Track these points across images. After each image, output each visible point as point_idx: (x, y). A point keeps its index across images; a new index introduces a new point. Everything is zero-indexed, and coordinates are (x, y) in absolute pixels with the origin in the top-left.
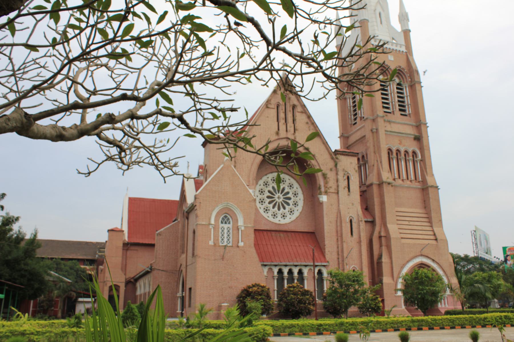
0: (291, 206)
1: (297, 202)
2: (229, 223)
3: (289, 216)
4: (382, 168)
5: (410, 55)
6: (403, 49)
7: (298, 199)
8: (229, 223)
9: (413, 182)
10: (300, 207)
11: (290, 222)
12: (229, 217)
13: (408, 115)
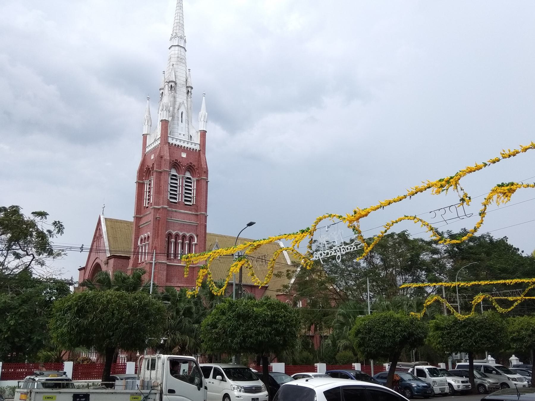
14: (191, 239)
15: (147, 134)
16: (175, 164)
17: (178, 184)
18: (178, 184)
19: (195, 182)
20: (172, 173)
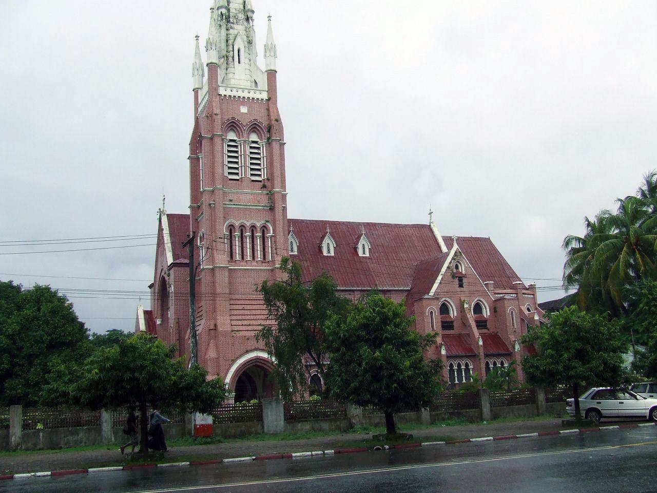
14: (244, 230)
15: (198, 88)
16: (254, 126)
17: (262, 153)
18: (262, 153)
19: (265, 147)
20: (251, 139)
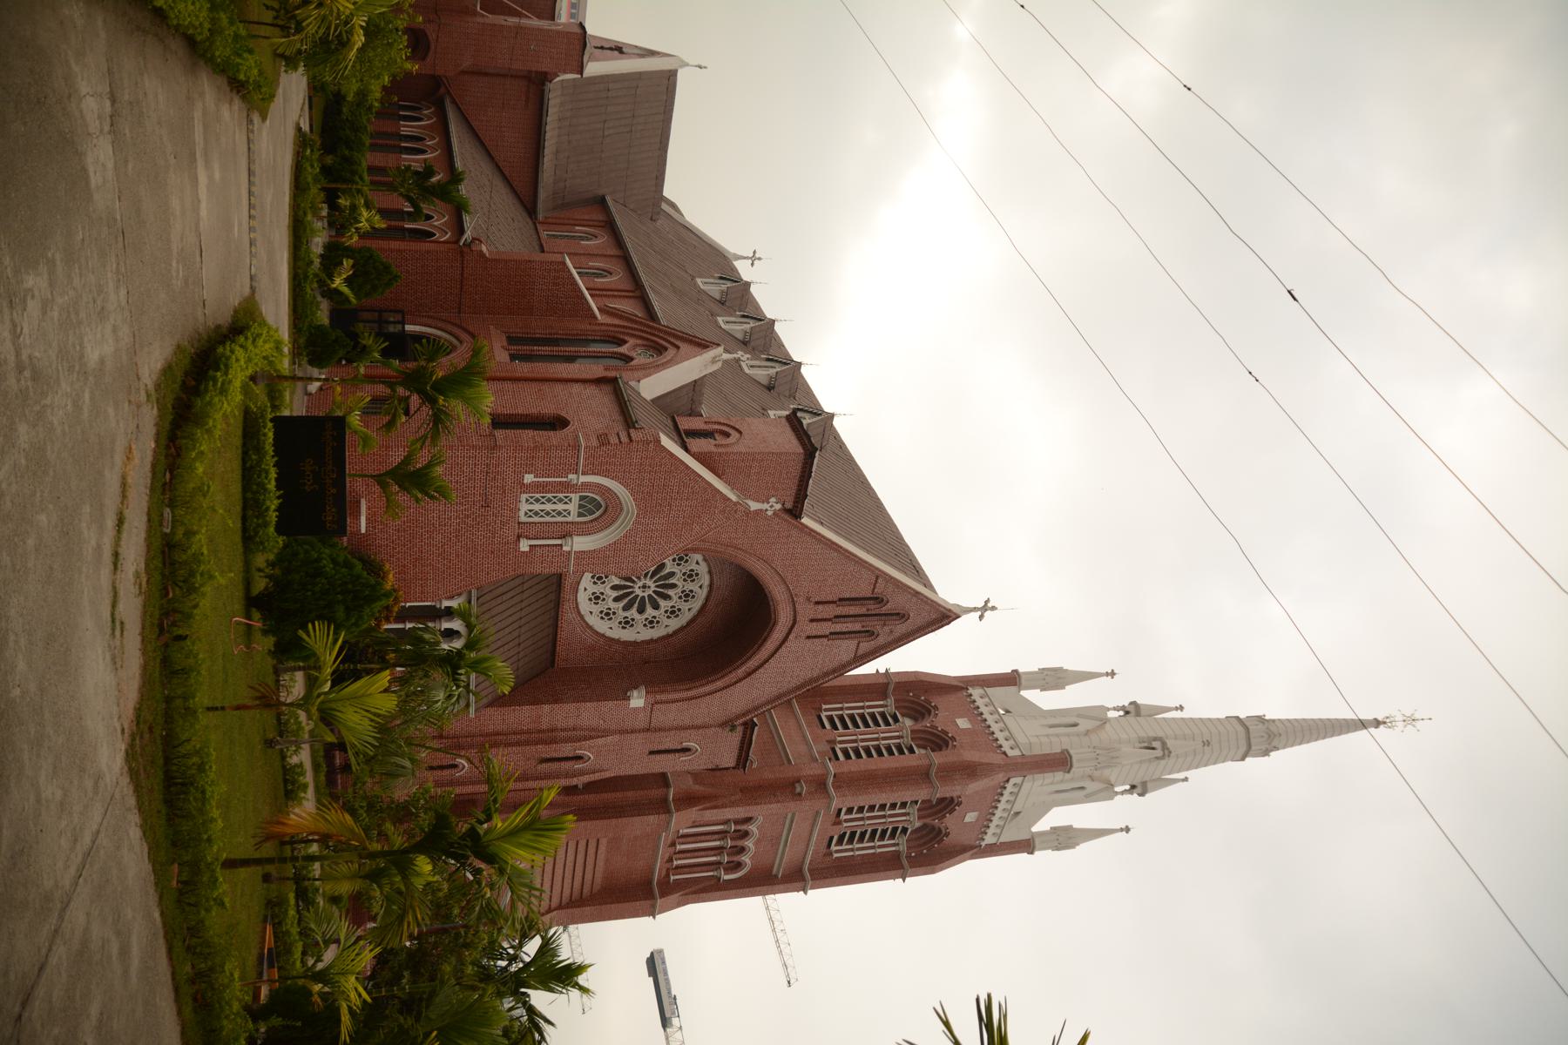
0: (622, 614)
1: (632, 625)
2: (580, 515)
3: (596, 609)
4: (686, 894)
5: (972, 855)
6: (989, 839)
7: (640, 627)
8: (580, 515)
9: (671, 850)
10: (618, 633)
11: (583, 613)
12: (598, 514)
13: (837, 820)
19: (894, 849)
